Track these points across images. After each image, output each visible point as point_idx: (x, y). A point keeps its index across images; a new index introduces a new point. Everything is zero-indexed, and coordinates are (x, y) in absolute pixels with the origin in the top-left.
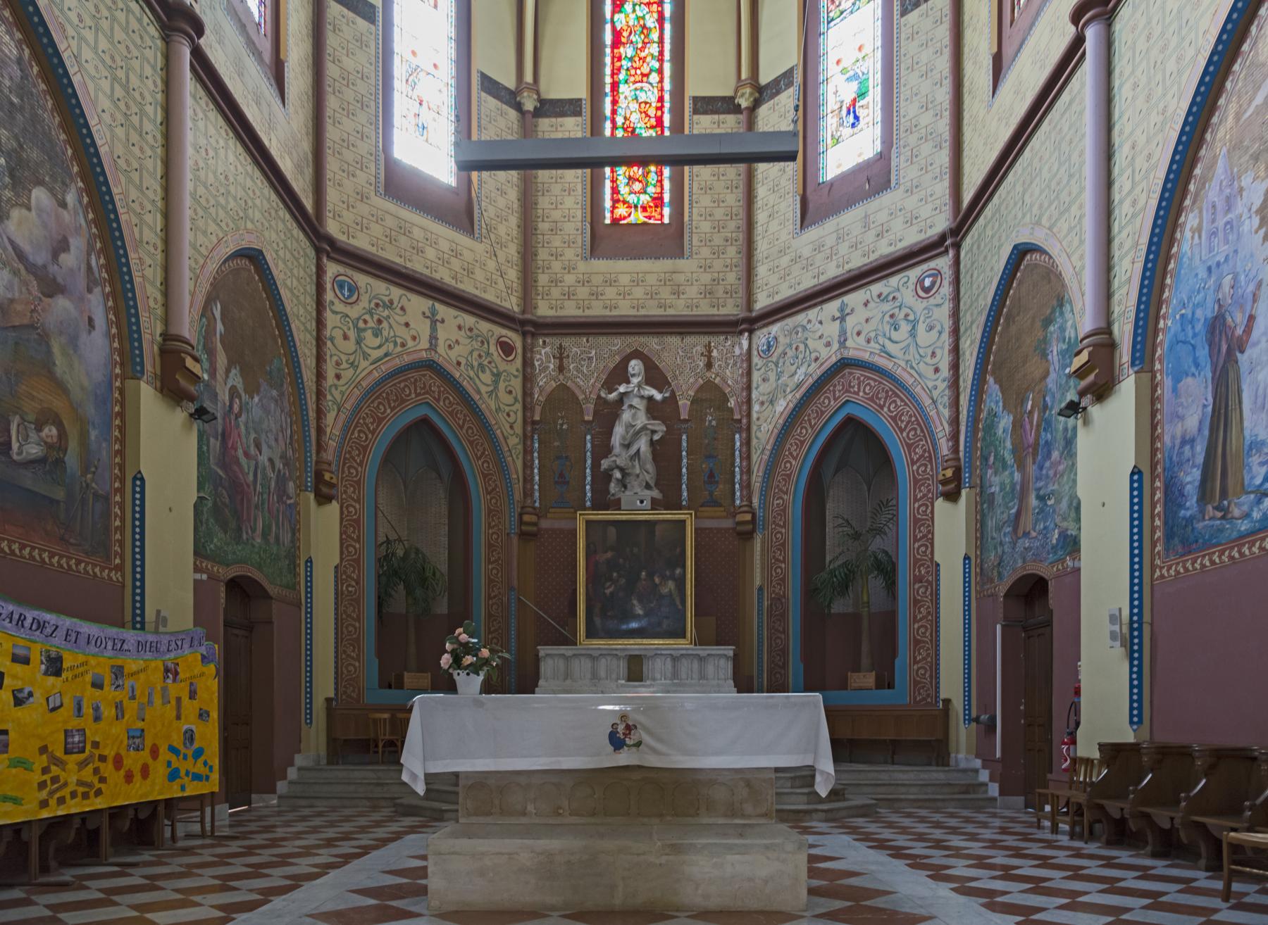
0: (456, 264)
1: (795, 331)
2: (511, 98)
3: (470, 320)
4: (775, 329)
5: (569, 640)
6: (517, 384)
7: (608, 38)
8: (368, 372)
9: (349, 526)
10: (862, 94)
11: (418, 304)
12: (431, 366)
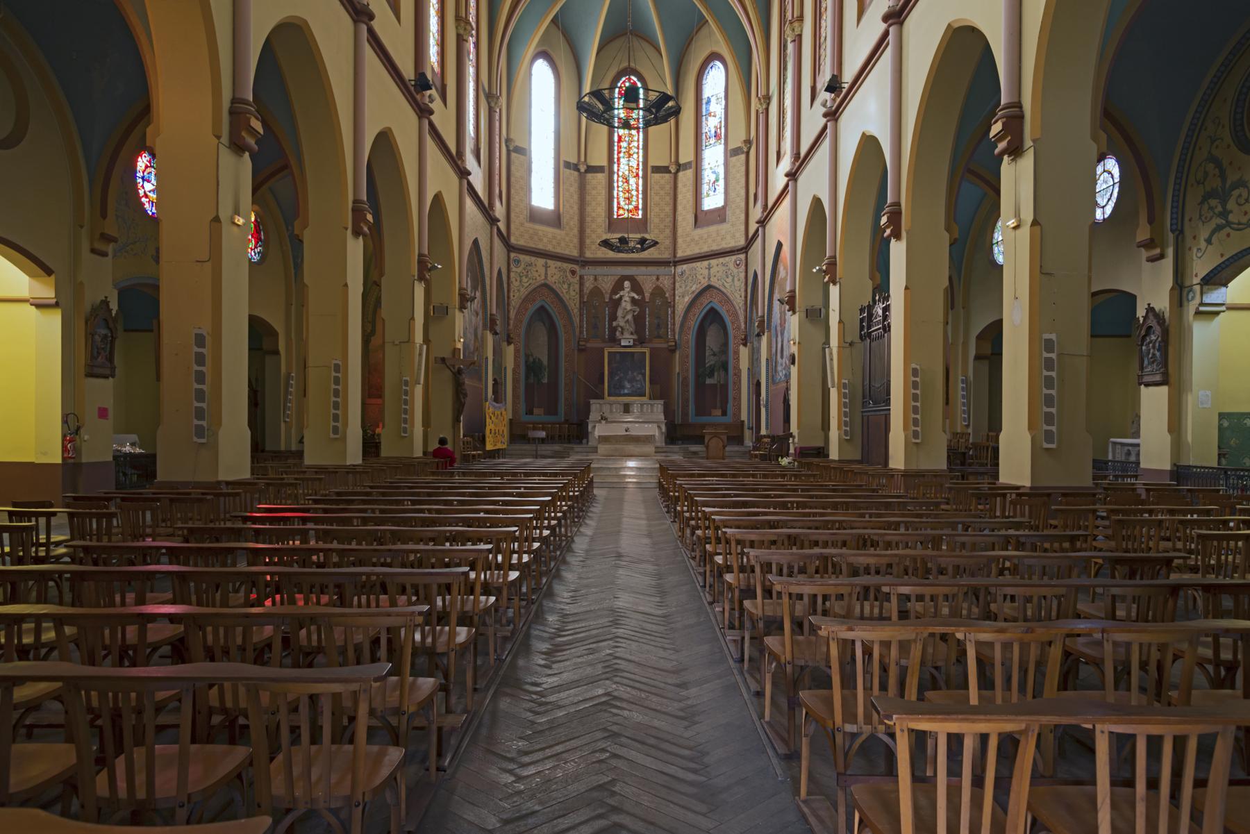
0: (554, 242)
1: (692, 269)
2: (576, 167)
3: (559, 264)
4: (685, 267)
5: (600, 396)
6: (577, 286)
7: (616, 139)
8: (524, 292)
9: (517, 351)
10: (717, 180)
11: (541, 261)
12: (545, 285)
